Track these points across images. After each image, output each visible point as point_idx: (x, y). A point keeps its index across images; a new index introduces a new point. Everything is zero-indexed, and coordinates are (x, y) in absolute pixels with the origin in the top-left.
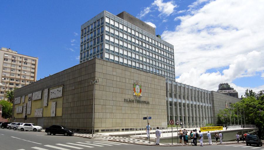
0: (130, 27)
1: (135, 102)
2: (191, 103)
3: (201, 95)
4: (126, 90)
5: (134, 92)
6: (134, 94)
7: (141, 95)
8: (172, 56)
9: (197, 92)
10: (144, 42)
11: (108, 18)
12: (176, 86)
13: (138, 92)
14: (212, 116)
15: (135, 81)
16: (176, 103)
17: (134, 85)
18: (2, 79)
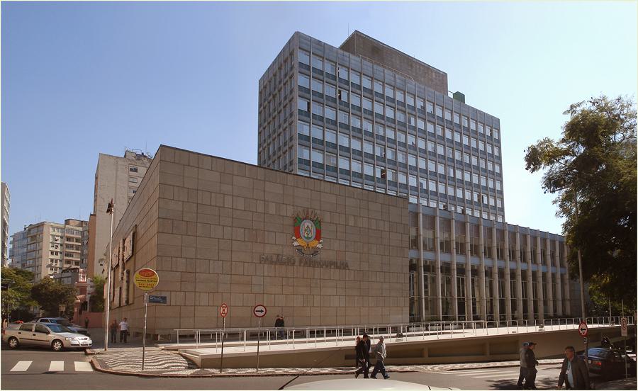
0: (430, 99)
1: (297, 263)
2: (497, 264)
3: (535, 245)
4: (266, 233)
5: (294, 238)
6: (295, 244)
7: (320, 246)
8: (496, 150)
9: (557, 243)
10: (429, 121)
11: (368, 76)
12: (501, 233)
13: (308, 238)
14: (568, 296)
15: (300, 209)
16: (446, 268)
17: (297, 222)
18: (636, 357)
